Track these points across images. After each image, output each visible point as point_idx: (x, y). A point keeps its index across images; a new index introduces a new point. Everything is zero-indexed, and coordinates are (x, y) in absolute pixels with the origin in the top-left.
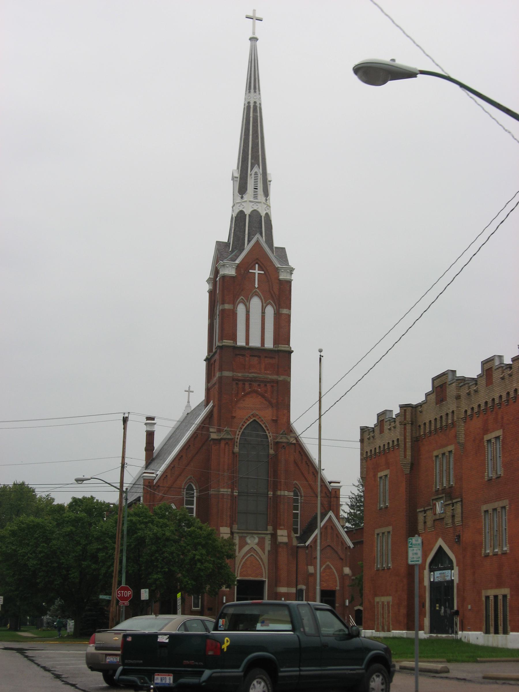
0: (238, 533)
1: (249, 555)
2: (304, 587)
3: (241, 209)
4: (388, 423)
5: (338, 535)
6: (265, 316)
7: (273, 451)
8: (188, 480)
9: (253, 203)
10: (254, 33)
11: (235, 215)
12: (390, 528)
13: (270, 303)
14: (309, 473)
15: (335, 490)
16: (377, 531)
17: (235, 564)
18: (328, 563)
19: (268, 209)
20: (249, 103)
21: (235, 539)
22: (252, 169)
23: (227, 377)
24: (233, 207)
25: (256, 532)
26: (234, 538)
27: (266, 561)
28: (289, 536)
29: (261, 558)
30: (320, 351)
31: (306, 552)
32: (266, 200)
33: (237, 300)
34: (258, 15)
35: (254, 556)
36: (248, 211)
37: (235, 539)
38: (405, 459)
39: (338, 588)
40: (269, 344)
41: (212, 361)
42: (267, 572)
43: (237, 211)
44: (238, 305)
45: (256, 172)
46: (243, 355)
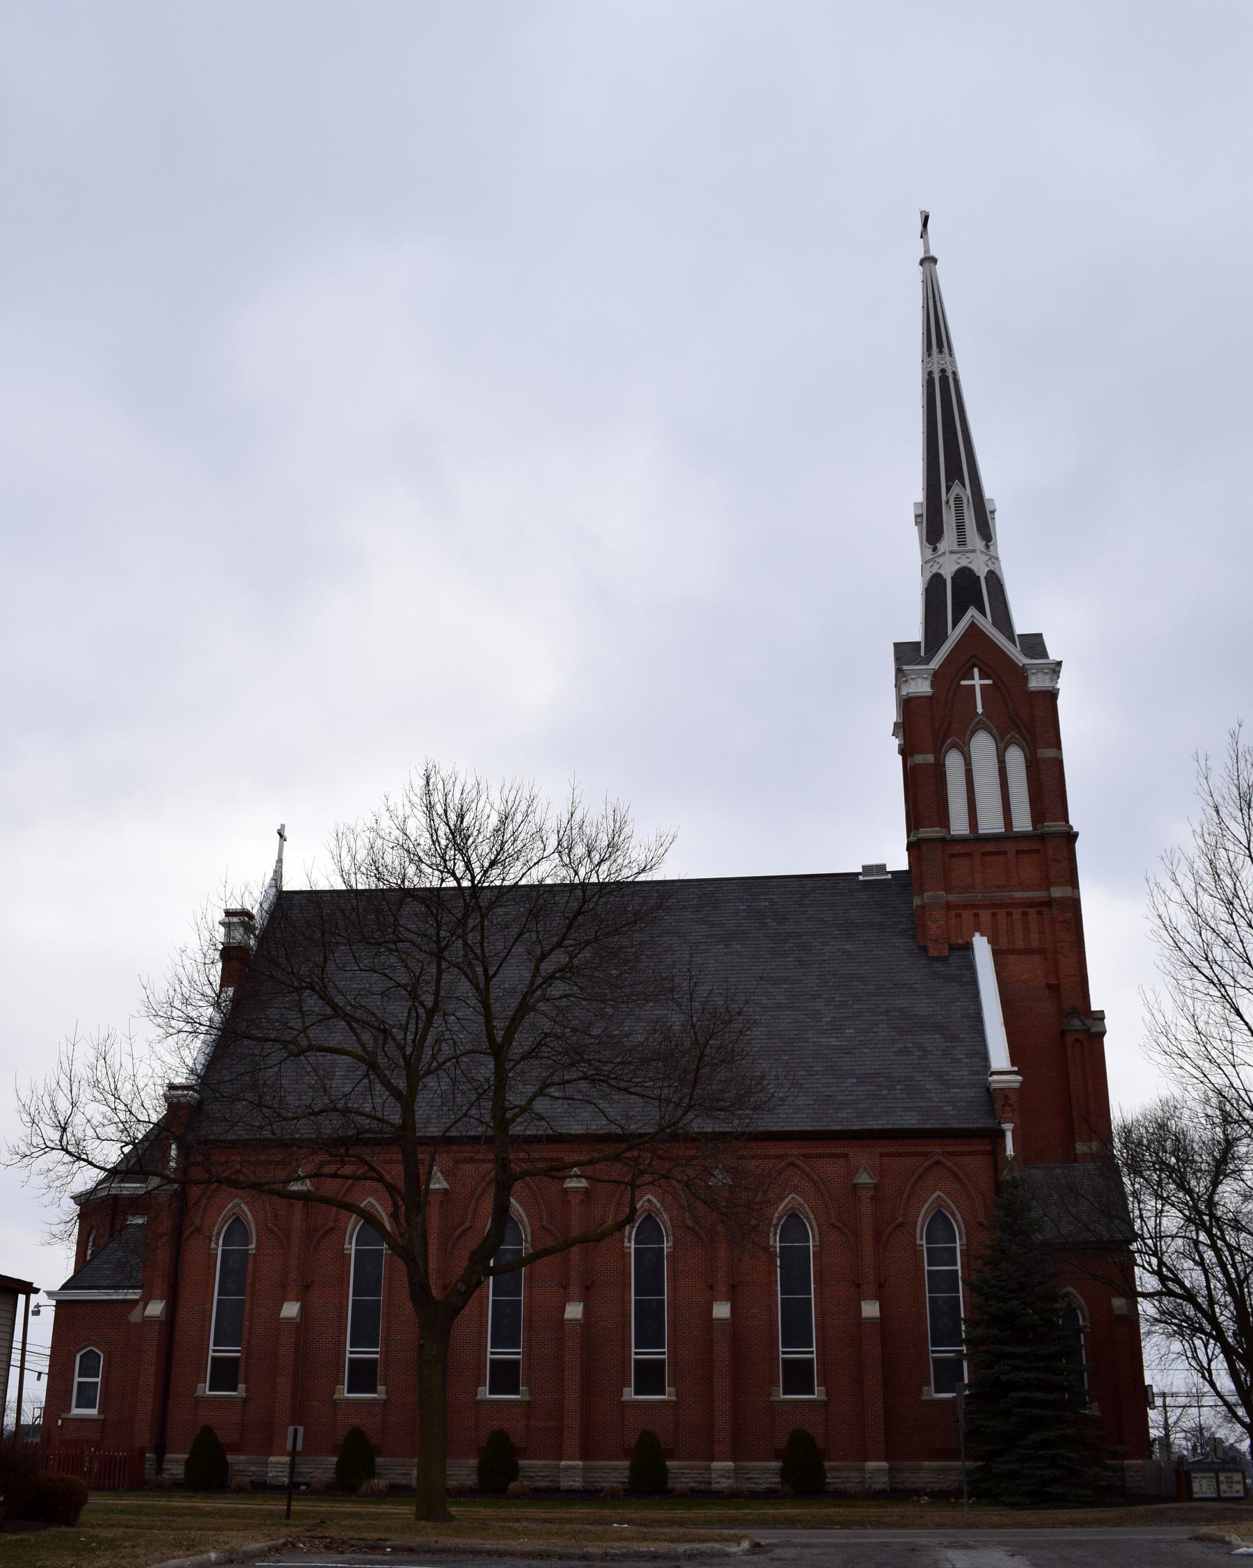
9: (959, 555)
10: (927, 250)
19: (993, 563)
20: (930, 373)
22: (948, 489)
32: (987, 547)
36: (948, 573)
40: (1023, 821)
43: (929, 576)
45: (958, 495)
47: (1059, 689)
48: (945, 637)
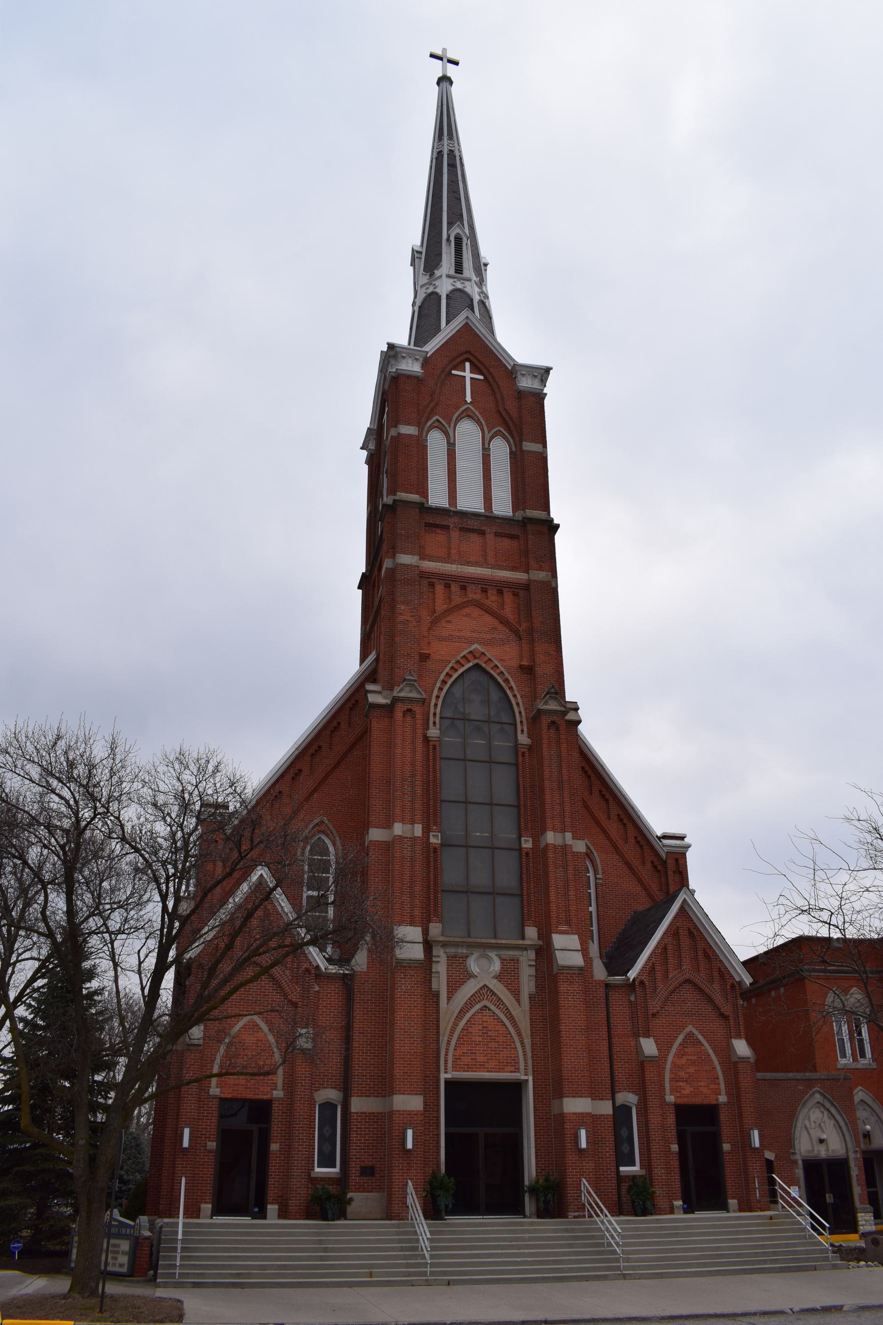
0: (444, 945)
1: (478, 1007)
6: (489, 455)
7: (527, 738)
8: (314, 827)
11: (418, 303)
14: (609, 818)
17: (438, 1033)
18: (690, 1028)
21: (438, 962)
23: (409, 424)
26: (434, 959)
27: (525, 1024)
29: (512, 1016)
33: (427, 421)
34: (451, 55)
35: (490, 1010)
37: (438, 962)
39: (723, 1099)
40: (503, 506)
42: (529, 1054)
43: (421, 296)
44: (428, 431)
46: (446, 528)
47: (546, 394)
48: (438, 330)
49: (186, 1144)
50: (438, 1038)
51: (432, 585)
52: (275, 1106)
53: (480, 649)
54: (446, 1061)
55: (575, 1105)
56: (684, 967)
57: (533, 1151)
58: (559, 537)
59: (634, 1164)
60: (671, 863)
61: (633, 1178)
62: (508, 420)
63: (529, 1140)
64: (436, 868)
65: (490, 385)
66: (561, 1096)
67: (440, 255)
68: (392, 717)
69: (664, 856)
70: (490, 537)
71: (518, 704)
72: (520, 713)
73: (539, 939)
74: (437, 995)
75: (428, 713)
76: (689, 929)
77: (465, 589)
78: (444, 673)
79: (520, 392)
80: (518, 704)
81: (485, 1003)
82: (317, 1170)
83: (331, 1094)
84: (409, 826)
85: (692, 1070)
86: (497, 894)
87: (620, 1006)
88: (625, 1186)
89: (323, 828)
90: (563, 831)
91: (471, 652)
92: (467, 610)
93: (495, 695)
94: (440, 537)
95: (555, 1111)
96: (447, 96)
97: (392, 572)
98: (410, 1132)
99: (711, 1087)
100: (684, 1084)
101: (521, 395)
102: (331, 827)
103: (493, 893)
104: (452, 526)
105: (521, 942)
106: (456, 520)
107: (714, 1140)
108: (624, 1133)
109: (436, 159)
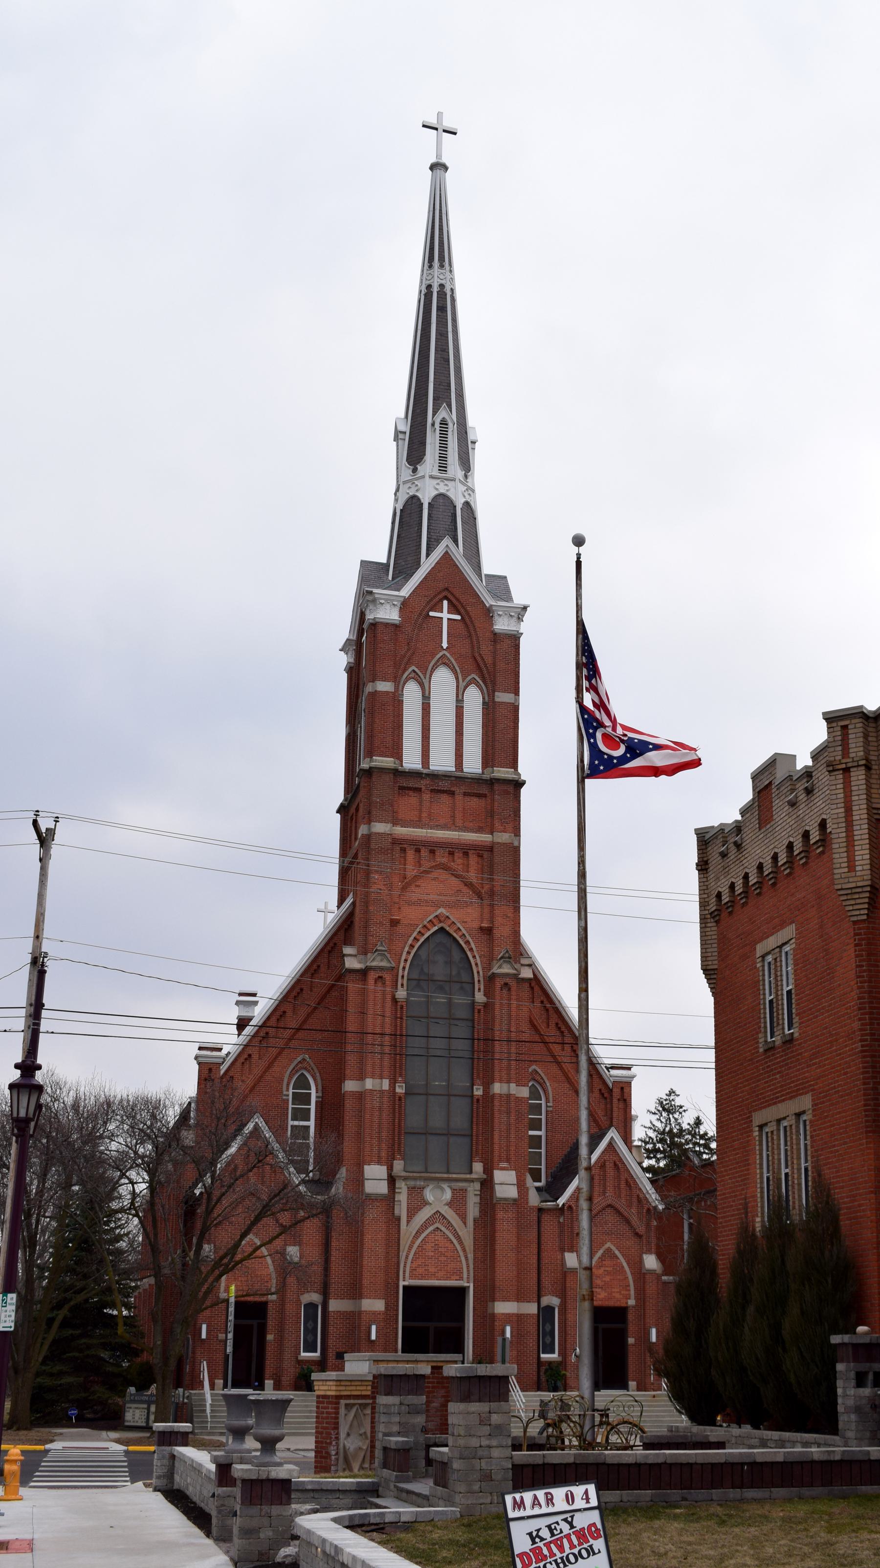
0: (405, 1179)
1: (431, 1228)
2: (555, 1301)
3: (411, 494)
4: (785, 789)
5: (631, 1183)
6: (463, 707)
7: (483, 997)
8: (297, 1065)
9: (438, 481)
10: (439, 155)
11: (400, 506)
12: (805, 1102)
13: (473, 681)
15: (621, 1085)
16: (758, 1118)
18: (608, 1245)
19: (469, 494)
20: (429, 287)
21: (400, 1193)
22: (435, 413)
24: (395, 494)
25: (445, 1176)
26: (397, 1191)
27: (469, 1242)
28: (521, 1185)
29: (459, 1236)
30: (579, 541)
31: (559, 1222)
32: (466, 477)
34: (447, 124)
35: (441, 1231)
37: (400, 1193)
38: (853, 874)
39: (631, 1302)
40: (473, 764)
41: (352, 810)
42: (471, 1266)
43: (403, 498)
44: (404, 684)
45: (444, 418)
46: (418, 790)
48: (417, 565)
49: (204, 1336)
50: (399, 1253)
51: (404, 850)
52: (270, 1306)
53: (445, 913)
54: (404, 1271)
55: (503, 1308)
56: (607, 1194)
57: (471, 1341)
58: (524, 791)
59: (553, 1352)
60: (616, 1092)
61: (550, 1363)
62: (482, 666)
63: (468, 1333)
64: (400, 1114)
65: (465, 623)
66: (493, 1300)
67: (423, 443)
68: (365, 980)
69: (611, 1085)
70: (459, 798)
71: (476, 964)
72: (478, 972)
73: (484, 1173)
74: (398, 1219)
75: (397, 976)
76: (615, 1163)
77: (434, 853)
78: (412, 938)
79: (495, 634)
80: (476, 964)
81: (437, 1225)
82: (303, 1354)
83: (315, 1297)
84: (378, 1081)
85: (607, 1279)
86: (451, 1135)
87: (550, 1226)
88: (543, 1369)
89: (305, 1065)
90: (509, 1082)
91: (437, 916)
92: (435, 874)
93: (456, 955)
94: (412, 800)
95: (490, 1311)
96: (440, 194)
97: (368, 837)
98: (374, 1328)
99: (622, 1292)
100: (600, 1290)
101: (496, 638)
102: (312, 1064)
103: (448, 1134)
104: (423, 788)
105: (468, 1176)
106: (427, 781)
107: (622, 1335)
108: (548, 1327)
109: (425, 295)
